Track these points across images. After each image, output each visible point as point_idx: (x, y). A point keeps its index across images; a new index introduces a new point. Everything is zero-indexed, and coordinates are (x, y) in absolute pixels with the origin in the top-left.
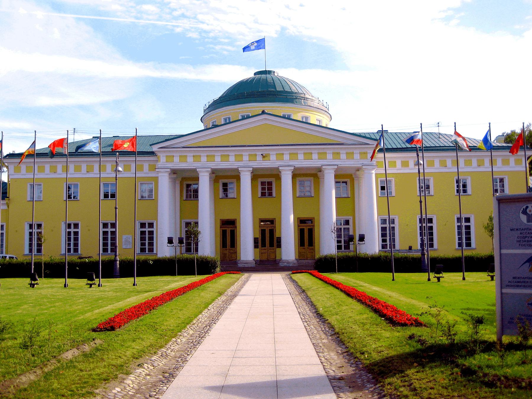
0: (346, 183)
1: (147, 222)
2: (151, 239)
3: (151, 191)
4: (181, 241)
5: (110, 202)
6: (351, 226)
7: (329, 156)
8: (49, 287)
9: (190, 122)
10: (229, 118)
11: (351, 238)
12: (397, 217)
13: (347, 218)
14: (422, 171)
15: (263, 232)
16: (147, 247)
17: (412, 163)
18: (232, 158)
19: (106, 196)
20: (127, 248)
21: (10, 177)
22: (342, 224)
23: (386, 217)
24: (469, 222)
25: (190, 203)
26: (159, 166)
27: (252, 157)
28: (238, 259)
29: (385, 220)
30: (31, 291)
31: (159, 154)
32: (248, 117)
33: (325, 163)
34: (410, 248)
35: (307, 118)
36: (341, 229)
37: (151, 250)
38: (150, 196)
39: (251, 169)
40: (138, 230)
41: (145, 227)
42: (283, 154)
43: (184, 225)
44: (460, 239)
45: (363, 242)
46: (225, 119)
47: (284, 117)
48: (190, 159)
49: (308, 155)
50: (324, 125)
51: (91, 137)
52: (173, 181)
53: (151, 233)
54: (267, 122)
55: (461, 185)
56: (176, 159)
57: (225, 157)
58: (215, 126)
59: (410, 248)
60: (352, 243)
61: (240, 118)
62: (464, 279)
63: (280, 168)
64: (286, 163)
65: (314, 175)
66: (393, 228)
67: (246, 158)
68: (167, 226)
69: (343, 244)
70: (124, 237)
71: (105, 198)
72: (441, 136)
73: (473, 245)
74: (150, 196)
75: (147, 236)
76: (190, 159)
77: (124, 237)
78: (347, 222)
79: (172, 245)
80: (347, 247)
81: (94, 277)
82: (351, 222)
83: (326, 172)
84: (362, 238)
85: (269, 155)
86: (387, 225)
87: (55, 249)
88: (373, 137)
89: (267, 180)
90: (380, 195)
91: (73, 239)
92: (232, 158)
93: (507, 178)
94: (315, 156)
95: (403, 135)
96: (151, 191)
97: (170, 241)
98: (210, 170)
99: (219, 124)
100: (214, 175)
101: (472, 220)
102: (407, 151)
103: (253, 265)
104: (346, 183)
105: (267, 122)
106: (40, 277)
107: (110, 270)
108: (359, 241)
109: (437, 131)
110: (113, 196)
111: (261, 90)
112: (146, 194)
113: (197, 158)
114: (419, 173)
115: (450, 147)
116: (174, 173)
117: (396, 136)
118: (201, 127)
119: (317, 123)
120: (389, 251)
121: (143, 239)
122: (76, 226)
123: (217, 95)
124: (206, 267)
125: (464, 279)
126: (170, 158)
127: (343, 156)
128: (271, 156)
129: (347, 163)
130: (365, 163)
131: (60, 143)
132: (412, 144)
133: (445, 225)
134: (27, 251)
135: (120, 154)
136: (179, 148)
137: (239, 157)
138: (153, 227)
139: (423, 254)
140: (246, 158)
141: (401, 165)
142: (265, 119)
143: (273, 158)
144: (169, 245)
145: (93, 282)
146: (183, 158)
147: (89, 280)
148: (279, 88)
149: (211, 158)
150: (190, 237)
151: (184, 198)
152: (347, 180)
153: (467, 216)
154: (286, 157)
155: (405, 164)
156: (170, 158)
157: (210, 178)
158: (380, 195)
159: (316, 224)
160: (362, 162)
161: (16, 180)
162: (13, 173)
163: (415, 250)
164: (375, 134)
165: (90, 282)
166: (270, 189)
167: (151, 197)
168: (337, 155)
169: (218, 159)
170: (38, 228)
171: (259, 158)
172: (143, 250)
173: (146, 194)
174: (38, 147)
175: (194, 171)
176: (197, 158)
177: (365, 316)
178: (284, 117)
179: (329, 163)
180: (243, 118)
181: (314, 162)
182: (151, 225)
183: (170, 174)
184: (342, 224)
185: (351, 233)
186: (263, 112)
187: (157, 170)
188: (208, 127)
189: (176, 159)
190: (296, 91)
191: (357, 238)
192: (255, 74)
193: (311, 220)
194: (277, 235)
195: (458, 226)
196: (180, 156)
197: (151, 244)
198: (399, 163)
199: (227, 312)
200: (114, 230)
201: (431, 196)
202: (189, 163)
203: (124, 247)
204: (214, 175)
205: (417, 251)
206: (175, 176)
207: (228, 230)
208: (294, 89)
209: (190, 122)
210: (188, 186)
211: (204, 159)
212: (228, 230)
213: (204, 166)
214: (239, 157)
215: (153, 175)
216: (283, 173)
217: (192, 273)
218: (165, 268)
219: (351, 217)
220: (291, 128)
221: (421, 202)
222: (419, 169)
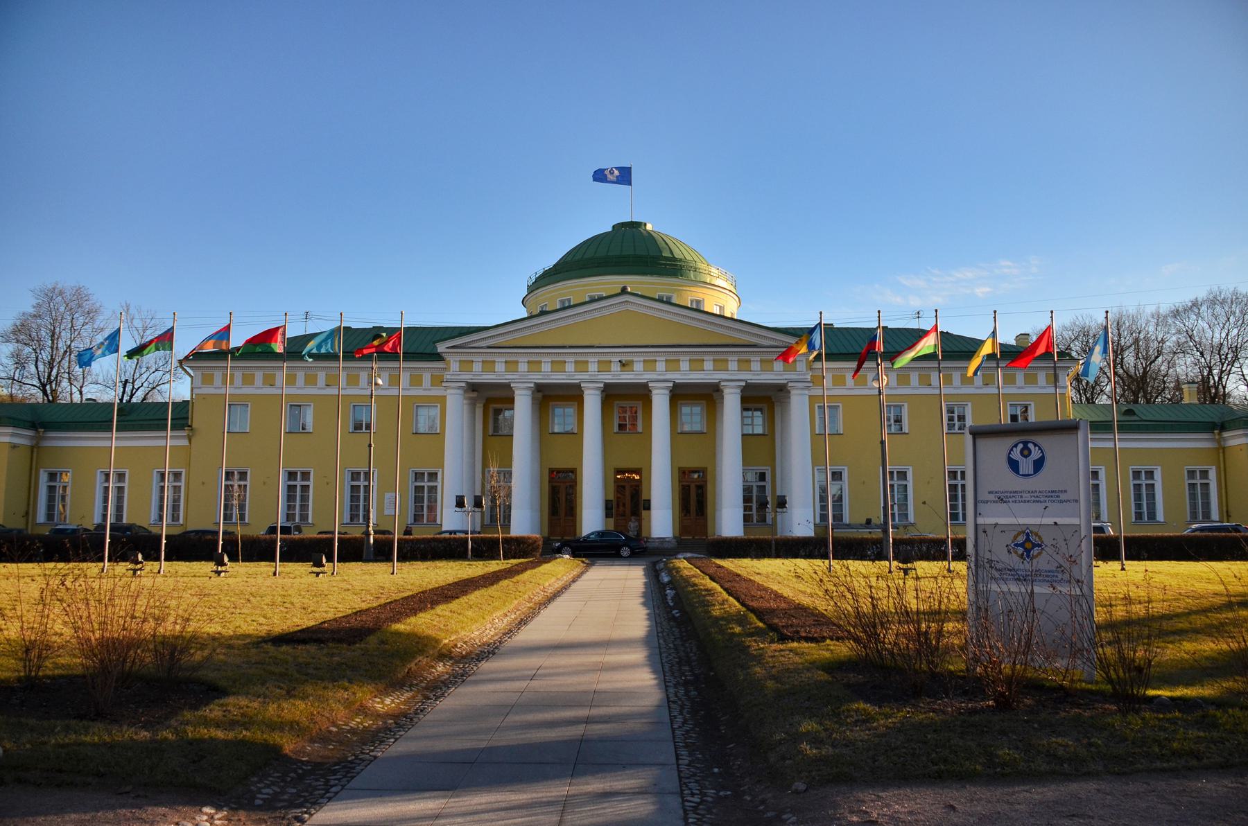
1: (1143, 468)
4: (478, 503)
5: (361, 438)
7: (733, 366)
8: (240, 573)
9: (501, 304)
10: (569, 300)
15: (620, 487)
18: (570, 367)
19: (358, 427)
20: (389, 510)
21: (196, 391)
27: (604, 366)
28: (644, 534)
30: (216, 580)
32: (601, 298)
33: (794, 377)
34: (869, 522)
35: (698, 302)
36: (956, 486)
41: (295, 479)
43: (411, 477)
44: (1139, 506)
46: (562, 302)
47: (660, 300)
48: (500, 367)
49: (696, 365)
50: (728, 314)
53: (433, 490)
54: (630, 307)
56: (477, 367)
57: (558, 365)
58: (543, 313)
59: (869, 522)
62: (1123, 569)
64: (659, 376)
65: (708, 396)
67: (593, 367)
68: (454, 477)
73: (1160, 517)
75: (424, 497)
76: (500, 367)
78: (762, 477)
82: (768, 477)
83: (793, 392)
84: (782, 503)
87: (267, 511)
91: (358, 499)
92: (570, 367)
94: (708, 365)
97: (460, 503)
101: (1158, 475)
103: (674, 544)
104: (761, 410)
105: (630, 307)
106: (233, 558)
107: (353, 551)
109: (916, 327)
110: (368, 427)
111: (630, 253)
113: (511, 365)
118: (523, 313)
119: (716, 311)
121: (1138, 497)
122: (306, 475)
124: (519, 548)
125: (1123, 569)
126: (466, 365)
127: (755, 366)
129: (762, 377)
131: (270, 335)
134: (154, 516)
139: (886, 531)
140: (593, 367)
141: (838, 380)
143: (638, 367)
146: (488, 365)
147: (315, 565)
148: (666, 254)
149: (534, 365)
150: (491, 503)
151: (491, 432)
152: (764, 400)
153: (901, 468)
154: (661, 366)
156: (466, 365)
157: (533, 399)
159: (709, 477)
161: (204, 397)
165: (316, 569)
166: (634, 418)
168: (744, 364)
169: (546, 367)
170: (240, 479)
171: (616, 367)
174: (854, 365)
175: (507, 387)
176: (511, 365)
177: (78, 661)
179: (732, 377)
181: (707, 374)
182: (433, 476)
186: (624, 291)
189: (477, 367)
190: (681, 257)
193: (703, 471)
194: (644, 497)
196: (576, 362)
197: (432, 509)
199: (537, 619)
202: (498, 374)
204: (540, 395)
205: (877, 527)
206: (475, 395)
207: (560, 491)
208: (677, 254)
209: (501, 304)
211: (523, 367)
212: (560, 491)
213: (522, 378)
214: (581, 366)
216: (654, 392)
217: (493, 556)
218: (449, 549)
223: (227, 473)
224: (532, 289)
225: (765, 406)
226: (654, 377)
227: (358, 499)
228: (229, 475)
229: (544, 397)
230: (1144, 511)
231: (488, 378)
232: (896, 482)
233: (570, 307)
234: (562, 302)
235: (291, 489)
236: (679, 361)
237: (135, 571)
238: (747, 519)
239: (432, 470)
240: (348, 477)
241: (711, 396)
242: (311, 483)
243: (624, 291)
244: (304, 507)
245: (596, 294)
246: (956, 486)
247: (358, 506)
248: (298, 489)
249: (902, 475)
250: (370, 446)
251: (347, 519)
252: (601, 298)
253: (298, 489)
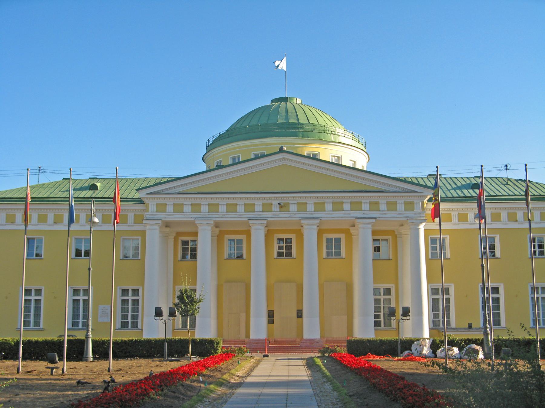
0: (387, 240)
1: (130, 288)
2: (135, 310)
3: (137, 248)
5: (83, 260)
6: (392, 297)
10: (239, 158)
11: (392, 313)
12: (43, 287)
13: (387, 286)
14: (483, 226)
16: (130, 320)
17: (520, 216)
19: (78, 254)
22: (382, 294)
23: (439, 285)
24: (122, 300)
25: (188, 263)
26: (148, 216)
29: (437, 289)
31: (147, 202)
32: (263, 156)
34: (470, 326)
37: (135, 325)
38: (136, 255)
39: (265, 222)
40: (372, 298)
41: (128, 295)
42: (306, 203)
45: (408, 318)
46: (234, 159)
50: (359, 167)
51: (60, 179)
52: (165, 237)
53: (135, 302)
55: (536, 244)
57: (338, 207)
58: (219, 167)
59: (470, 326)
60: (394, 318)
61: (252, 157)
63: (197, 222)
66: (498, 299)
68: (157, 293)
69: (382, 319)
70: (101, 307)
71: (278, 256)
72: (509, 182)
74: (136, 255)
77: (101, 307)
78: (388, 292)
79: (161, 318)
80: (388, 324)
81: (57, 359)
82: (393, 292)
85: (288, 204)
86: (440, 296)
88: (422, 182)
89: (334, 236)
90: (430, 258)
91: (80, 314)
93: (43, 237)
95: (460, 180)
96: (137, 248)
97: (159, 313)
98: (212, 222)
99: (225, 164)
100: (267, 229)
101: (501, 291)
102: (466, 200)
108: (402, 315)
109: (504, 176)
110: (87, 254)
112: (131, 253)
114: (480, 229)
115: (503, 196)
116: (166, 227)
117: (449, 180)
119: (350, 164)
120: (442, 329)
121: (124, 310)
122: (38, 292)
123: (223, 129)
128: (291, 206)
130: (410, 215)
132: (476, 191)
133: (517, 296)
135: (96, 201)
136: (173, 194)
137: (356, 206)
138: (138, 295)
139: (486, 334)
142: (284, 158)
144: (157, 318)
145: (56, 365)
151: (325, 255)
153: (495, 285)
155: (512, 218)
158: (430, 258)
160: (407, 215)
162: (5, 223)
163: (476, 329)
164: (425, 179)
166: (289, 248)
167: (135, 257)
171: (275, 208)
172: (124, 325)
173: (131, 253)
178: (308, 157)
180: (257, 157)
182: (136, 292)
183: (160, 227)
184: (382, 294)
185: (393, 305)
187: (144, 222)
188: (211, 168)
190: (324, 124)
191: (400, 312)
192: (272, 102)
195: (375, 300)
197: (135, 317)
198: (504, 216)
200: (86, 298)
201: (497, 258)
202: (187, 214)
203: (100, 320)
205: (478, 329)
210: (185, 243)
215: (138, 227)
219: (394, 285)
220: (351, 179)
221: (482, 266)
222: (480, 224)
223: (26, 290)
224: (209, 148)
225: (390, 238)
226: (251, 215)
227: (80, 314)
228: (28, 292)
229: (220, 231)
230: (129, 320)
231: (178, 217)
232: (491, 296)
233: (239, 163)
234: (234, 159)
235: (76, 302)
236: (324, 203)
237: (52, 369)
238: (377, 324)
239: (135, 287)
240: (119, 293)
241: (349, 230)
242: (42, 298)
243: (281, 150)
244: (37, 316)
245: (259, 152)
246: (78, 301)
247: (78, 315)
248: (33, 302)
249: (496, 290)
250: (89, 270)
251: (119, 325)
252: (263, 156)
253: (33, 302)
